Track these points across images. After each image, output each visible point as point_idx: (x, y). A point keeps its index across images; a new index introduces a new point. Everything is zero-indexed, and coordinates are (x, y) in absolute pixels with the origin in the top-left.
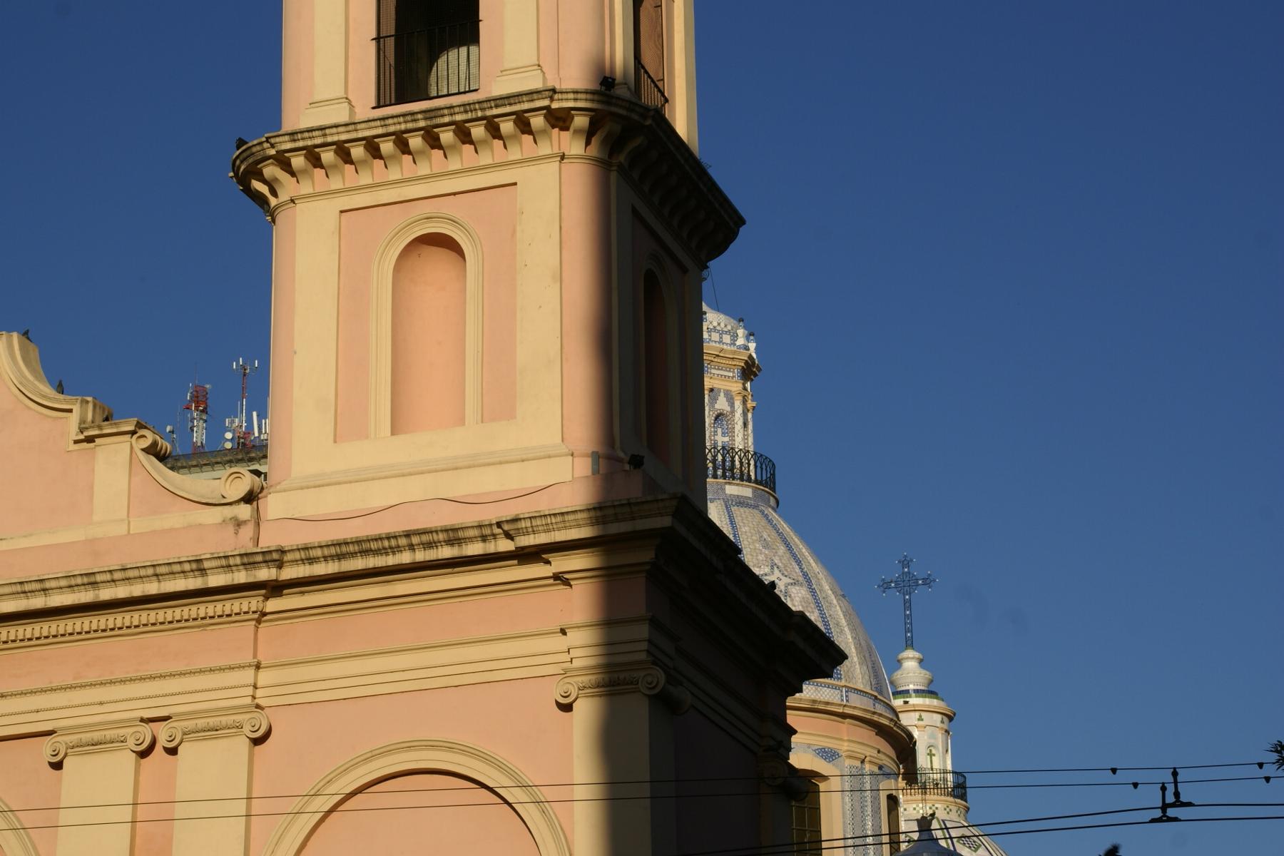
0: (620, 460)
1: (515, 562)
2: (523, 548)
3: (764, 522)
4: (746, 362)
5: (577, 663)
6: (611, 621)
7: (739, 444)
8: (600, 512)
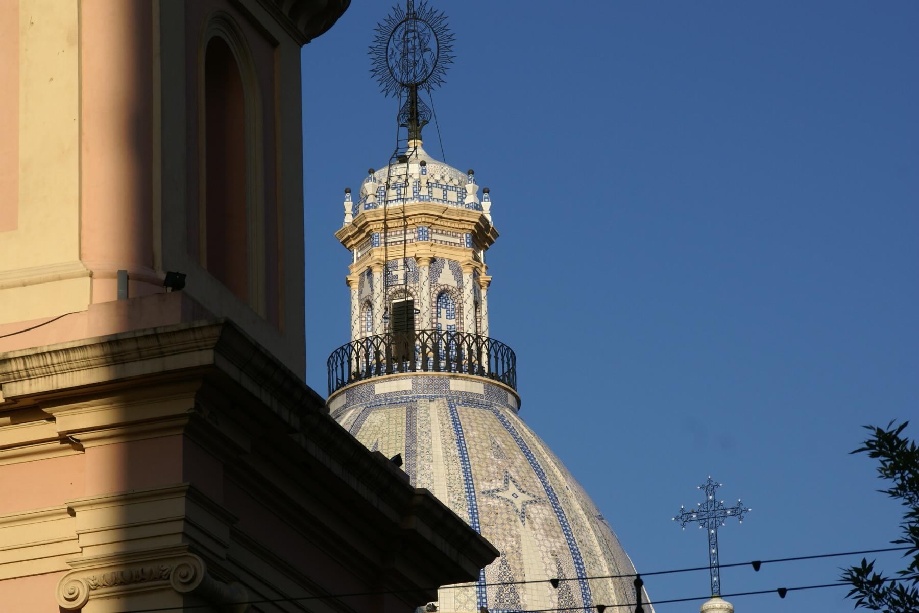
0: (156, 282)
1: (8, 419)
2: (15, 399)
3: (498, 425)
4: (477, 225)
5: (88, 553)
6: (131, 496)
7: (468, 327)
8: (113, 348)
